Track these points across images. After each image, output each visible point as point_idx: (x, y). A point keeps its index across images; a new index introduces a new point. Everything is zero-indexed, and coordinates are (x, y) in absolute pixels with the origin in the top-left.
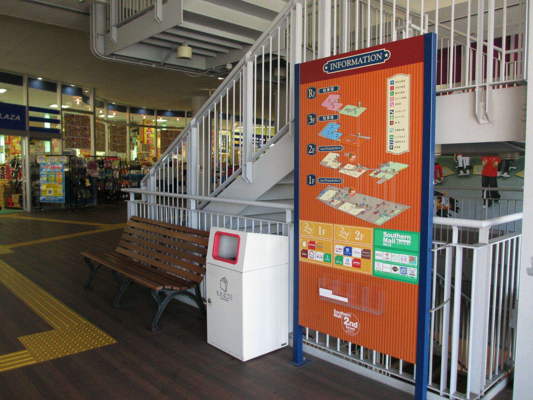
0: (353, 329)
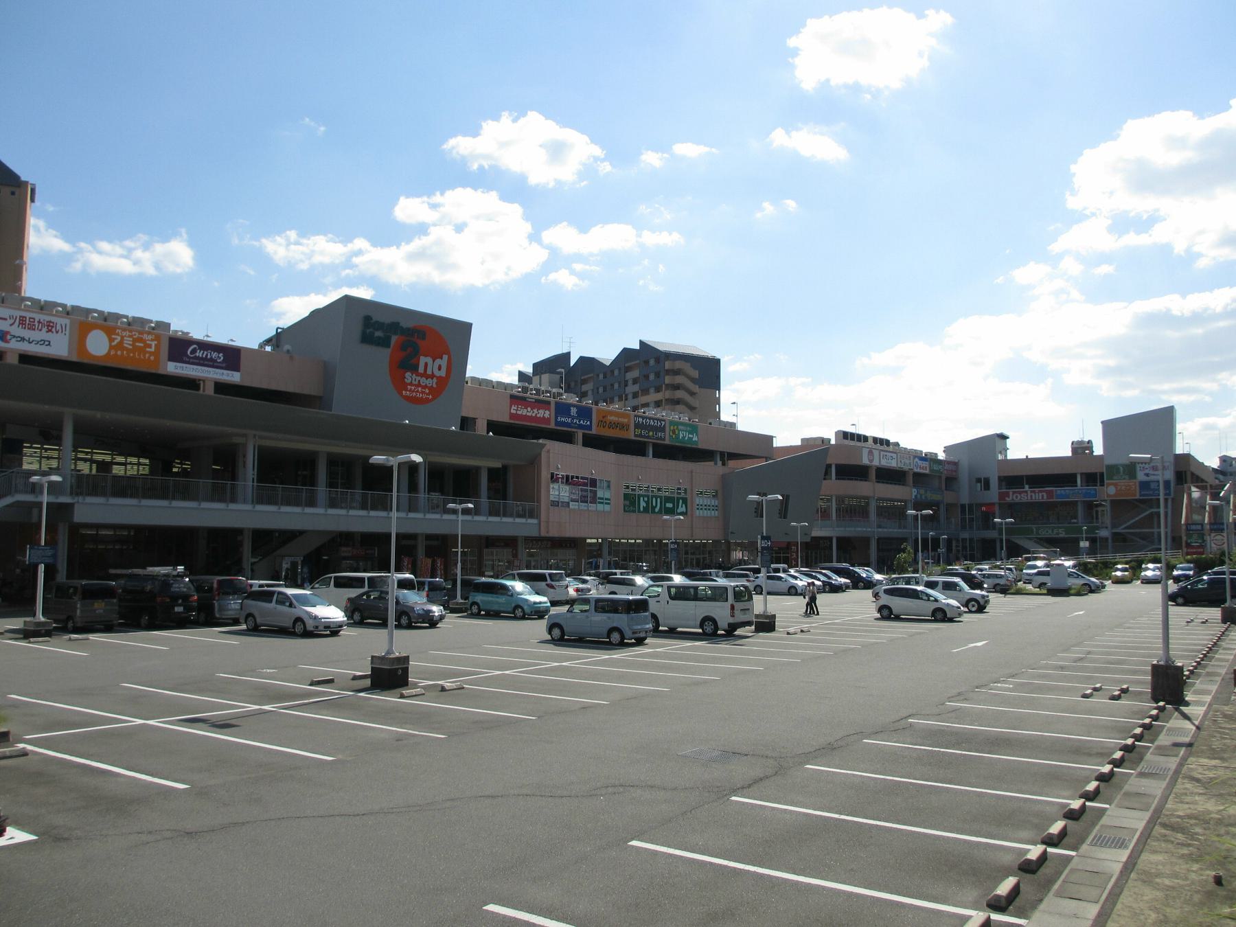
0: (429, 382)
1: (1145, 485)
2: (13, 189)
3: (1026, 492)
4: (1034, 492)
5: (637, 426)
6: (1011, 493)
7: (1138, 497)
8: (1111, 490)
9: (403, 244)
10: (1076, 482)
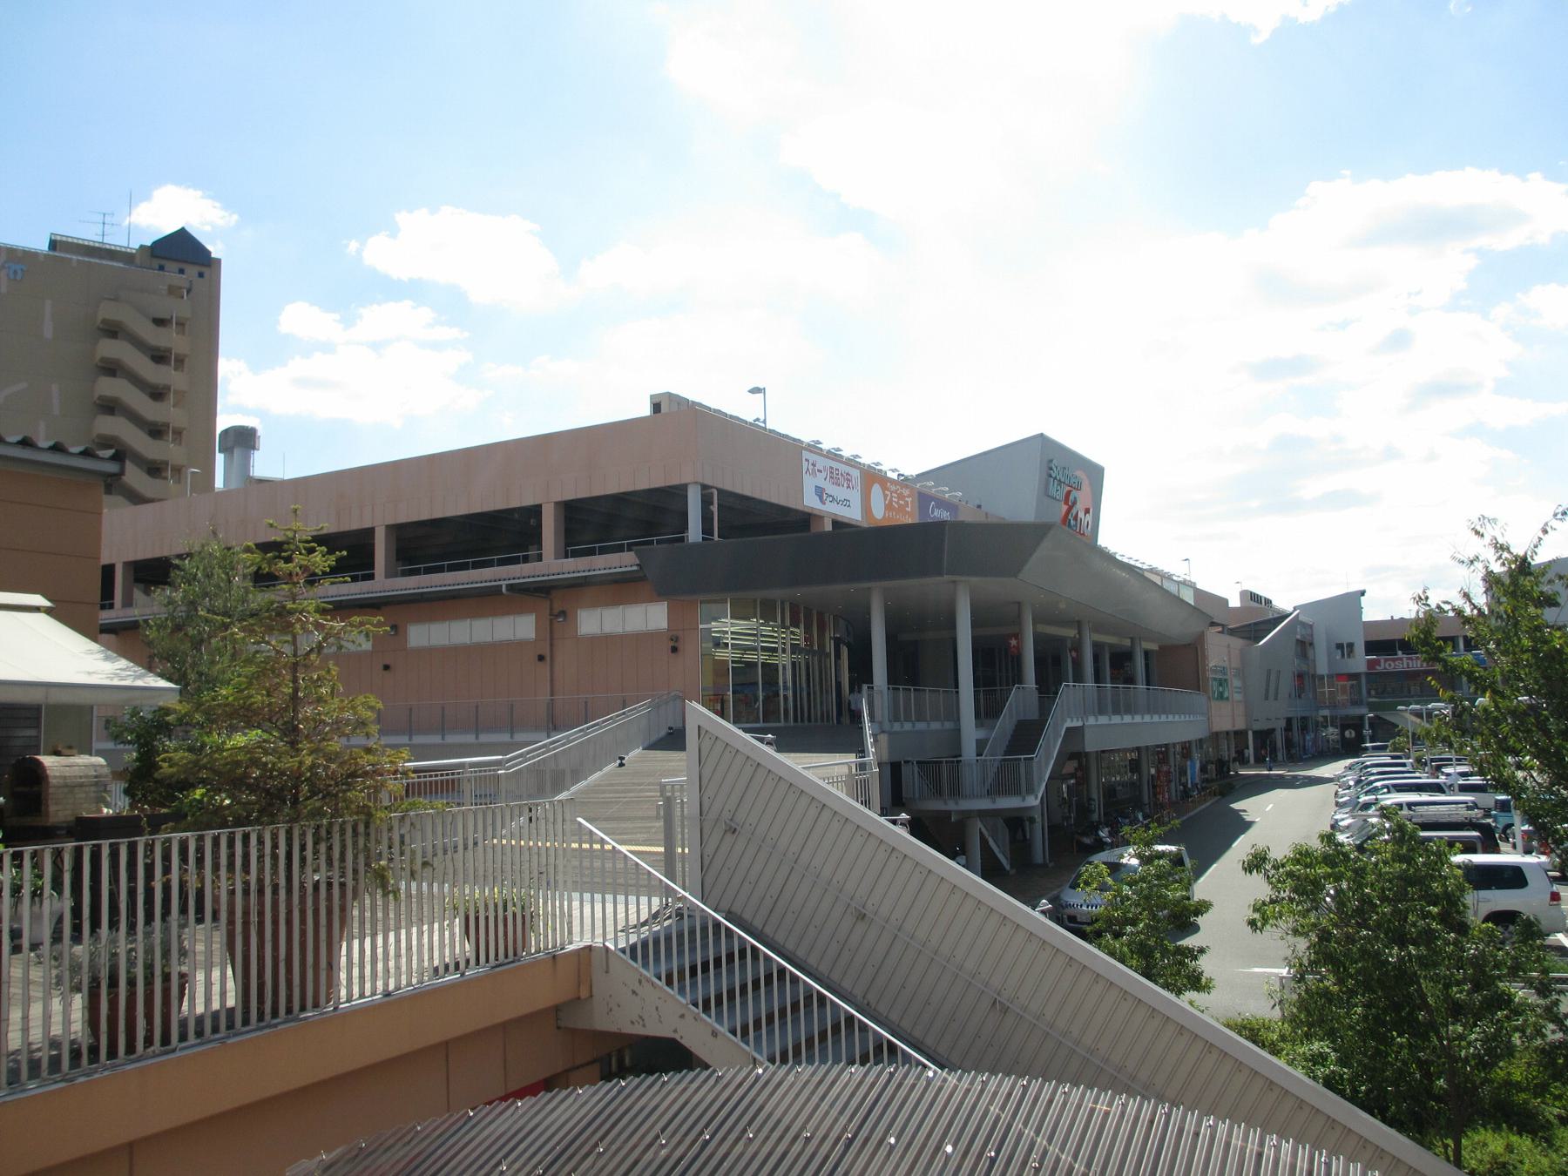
3: (1401, 659)
4: (1411, 659)
6: (1382, 661)
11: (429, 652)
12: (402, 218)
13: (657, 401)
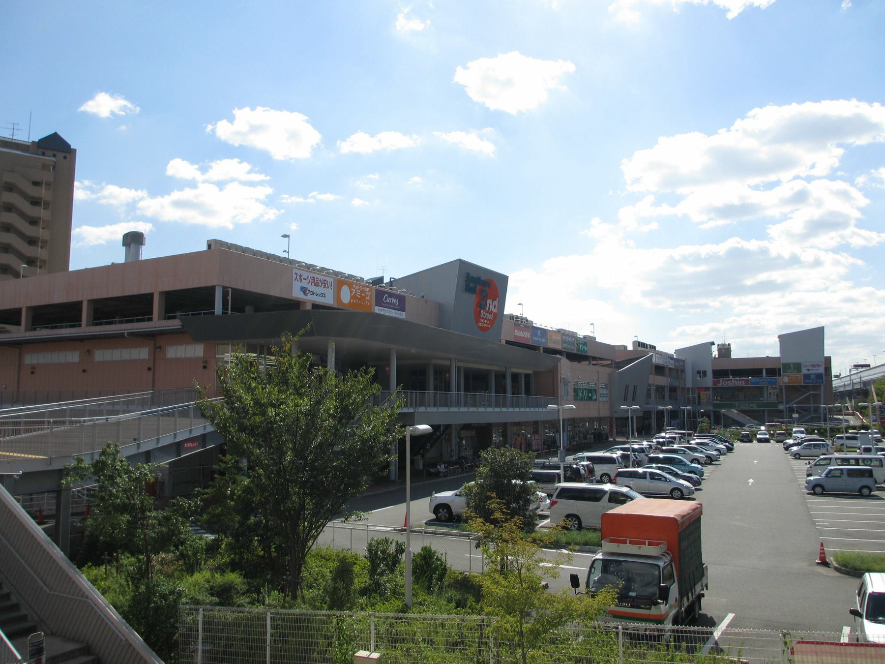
1: (807, 376)
2: (65, 155)
3: (731, 380)
5: (564, 341)
7: (803, 384)
8: (786, 379)
9: (175, 190)
10: (762, 374)
11: (178, 360)
12: (237, 112)
13: (209, 243)
